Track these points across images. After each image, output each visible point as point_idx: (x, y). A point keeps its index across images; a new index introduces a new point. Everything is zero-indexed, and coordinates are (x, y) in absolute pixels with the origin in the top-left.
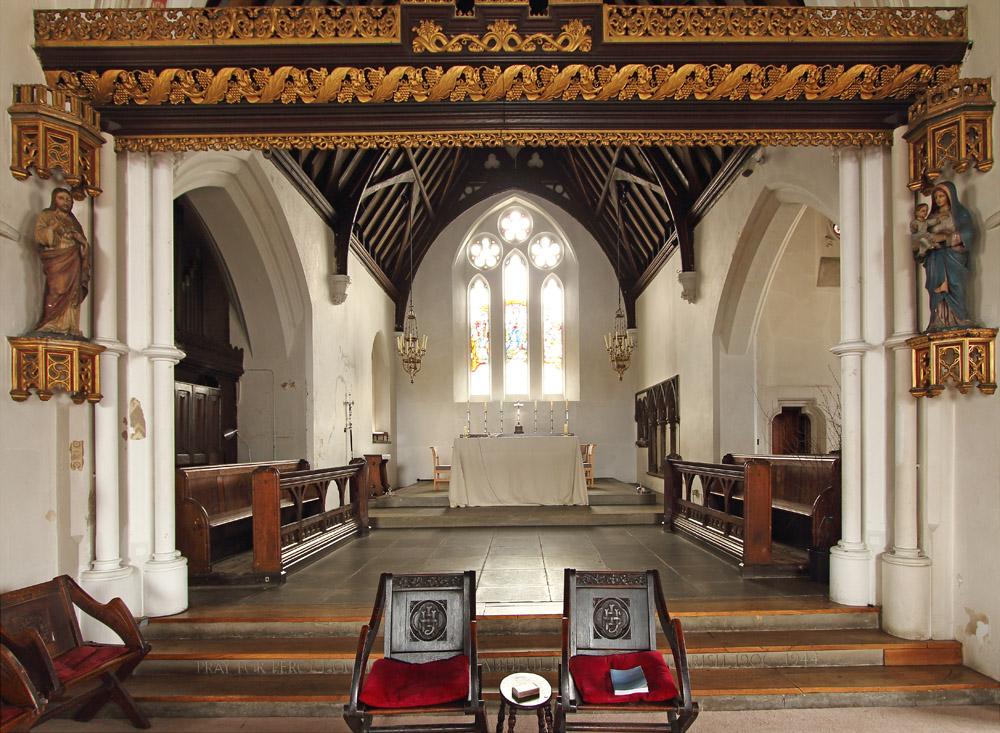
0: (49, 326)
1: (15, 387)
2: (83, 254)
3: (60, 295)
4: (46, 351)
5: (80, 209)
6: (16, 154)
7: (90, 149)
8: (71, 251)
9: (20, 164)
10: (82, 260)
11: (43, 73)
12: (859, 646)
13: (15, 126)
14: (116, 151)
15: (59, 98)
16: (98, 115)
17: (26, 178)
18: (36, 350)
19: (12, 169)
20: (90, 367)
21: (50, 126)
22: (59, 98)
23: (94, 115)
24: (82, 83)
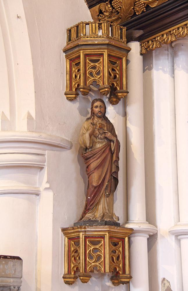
0: (89, 215)
1: (66, 272)
2: (113, 149)
3: (95, 187)
4: (86, 237)
5: (112, 113)
6: (68, 82)
7: (118, 60)
8: (103, 150)
9: (71, 89)
10: (112, 154)
11: (89, 11)
12: (67, 262)
13: (68, 60)
14: (141, 54)
15: (94, 27)
16: (124, 30)
17: (75, 98)
18: (79, 237)
19: (66, 94)
20: (121, 249)
21: (88, 52)
22: (94, 27)
23: (121, 29)
24: (113, 8)
